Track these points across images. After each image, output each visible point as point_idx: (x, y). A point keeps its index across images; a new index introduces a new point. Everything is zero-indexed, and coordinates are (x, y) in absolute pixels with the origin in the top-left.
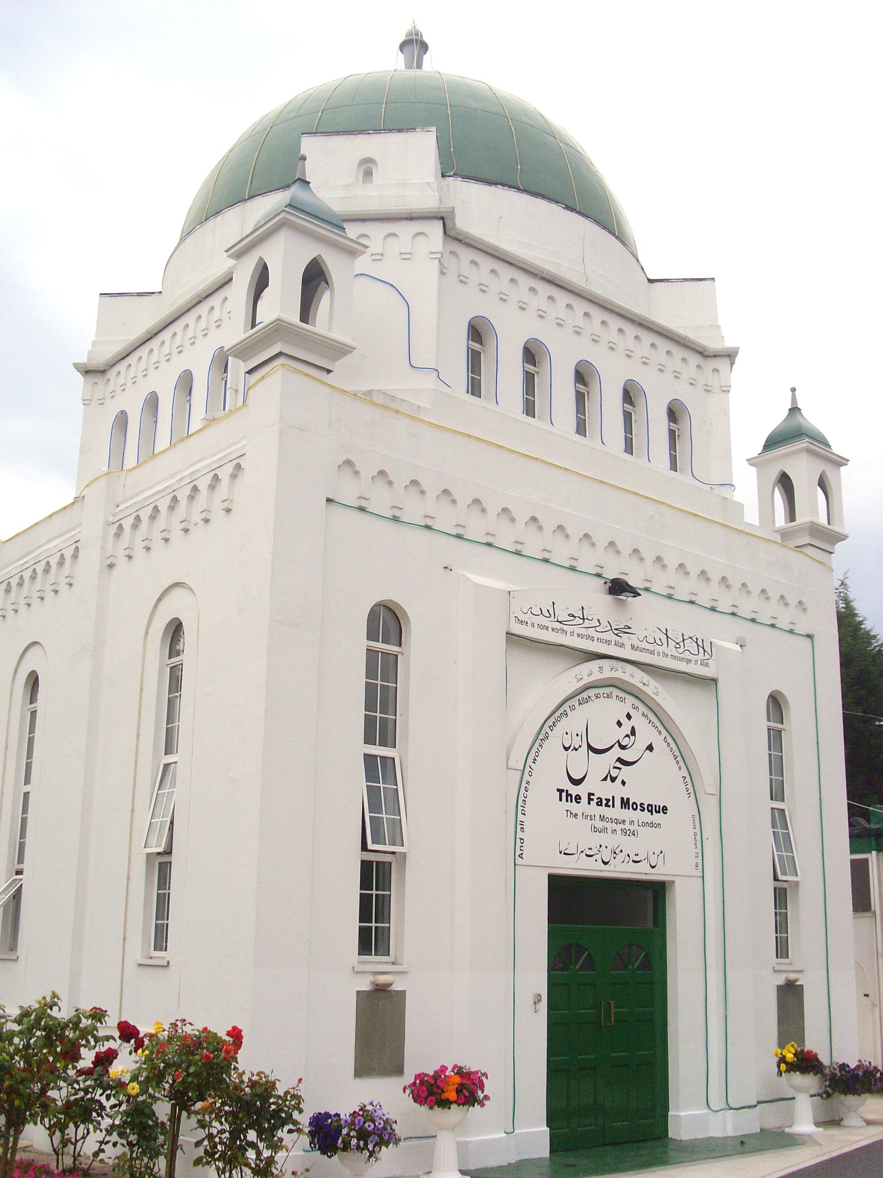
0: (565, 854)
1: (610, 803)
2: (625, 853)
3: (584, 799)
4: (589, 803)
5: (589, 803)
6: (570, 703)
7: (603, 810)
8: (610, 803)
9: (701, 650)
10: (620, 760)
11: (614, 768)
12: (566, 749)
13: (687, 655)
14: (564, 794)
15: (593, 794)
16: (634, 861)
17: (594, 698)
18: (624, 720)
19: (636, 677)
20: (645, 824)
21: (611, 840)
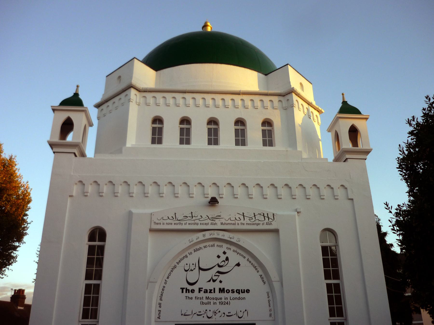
1: (213, 291)
7: (208, 295)
8: (213, 291)
10: (218, 272)
11: (215, 276)
12: (186, 271)
13: (257, 222)
16: (227, 316)
20: (234, 299)
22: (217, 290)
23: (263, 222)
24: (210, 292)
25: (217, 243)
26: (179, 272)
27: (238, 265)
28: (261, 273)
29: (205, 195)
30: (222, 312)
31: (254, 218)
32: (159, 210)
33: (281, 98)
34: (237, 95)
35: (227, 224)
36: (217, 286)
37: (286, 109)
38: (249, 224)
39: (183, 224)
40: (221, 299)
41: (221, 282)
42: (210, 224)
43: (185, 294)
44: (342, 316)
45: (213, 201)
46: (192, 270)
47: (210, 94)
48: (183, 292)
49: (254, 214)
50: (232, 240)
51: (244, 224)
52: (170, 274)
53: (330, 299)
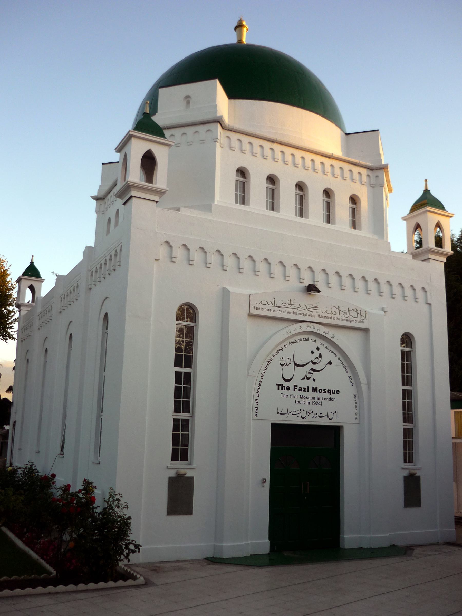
1: (307, 390)
7: (302, 393)
8: (307, 390)
10: (312, 369)
11: (309, 373)
12: (282, 365)
13: (351, 318)
16: (319, 417)
20: (326, 399)
22: (311, 389)
23: (356, 319)
24: (304, 391)
25: (311, 337)
26: (275, 366)
27: (330, 363)
28: (349, 374)
29: (300, 280)
30: (314, 412)
31: (348, 313)
32: (257, 292)
33: (370, 172)
34: (327, 159)
35: (324, 317)
36: (310, 384)
37: (373, 187)
38: (343, 320)
39: (282, 312)
40: (314, 398)
41: (314, 380)
42: (308, 315)
43: (281, 391)
44: (189, 412)
45: (311, 289)
46: (288, 365)
47: (299, 151)
48: (278, 389)
49: (348, 309)
50: (326, 335)
51: (339, 319)
52: (266, 367)
53: (177, 391)
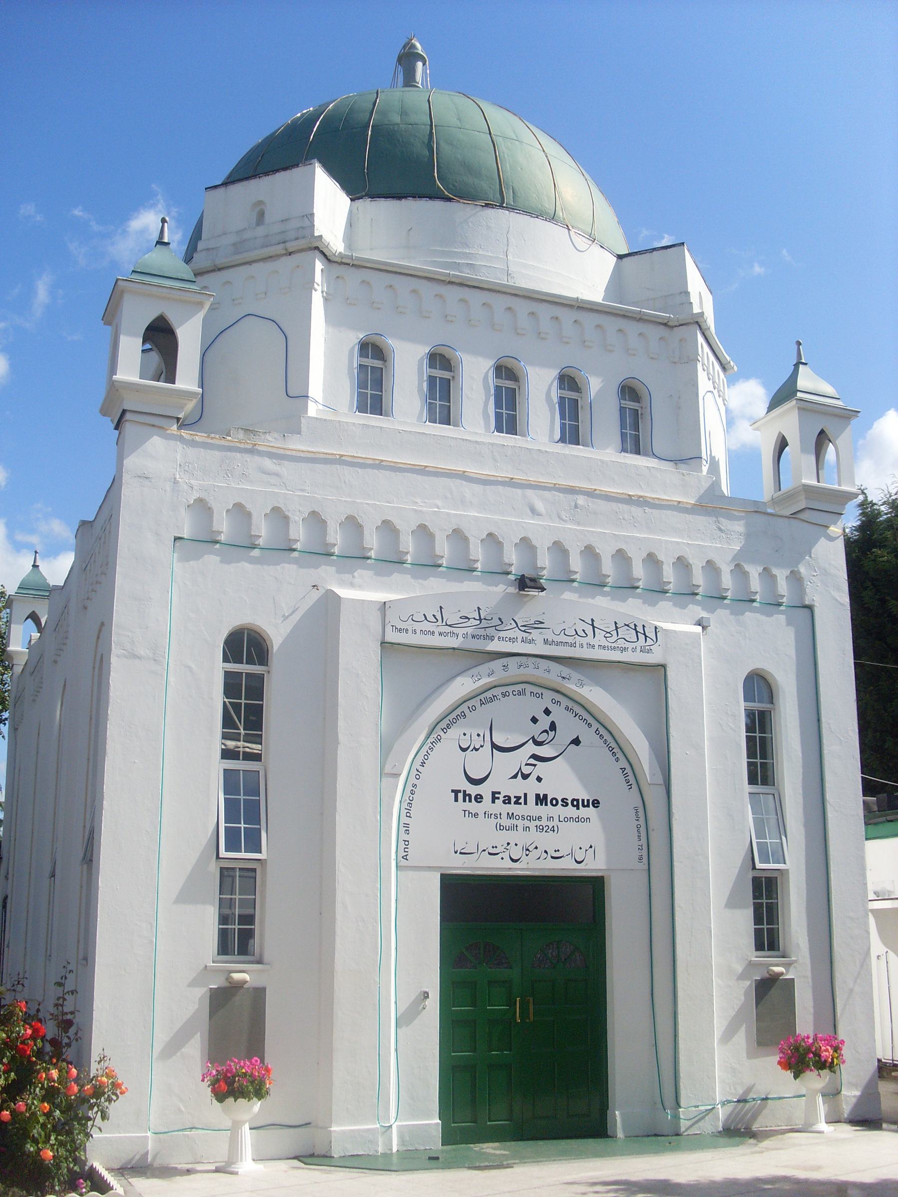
0: (461, 853)
2: (541, 849)
3: (488, 797)
4: (493, 802)
5: (493, 802)
6: (470, 704)
7: (512, 808)
9: (642, 637)
10: (534, 757)
11: (527, 764)
12: (464, 750)
14: (460, 795)
15: (499, 793)
16: (552, 857)
17: (500, 696)
18: (541, 716)
19: (553, 674)
20: (568, 819)
21: (520, 838)
